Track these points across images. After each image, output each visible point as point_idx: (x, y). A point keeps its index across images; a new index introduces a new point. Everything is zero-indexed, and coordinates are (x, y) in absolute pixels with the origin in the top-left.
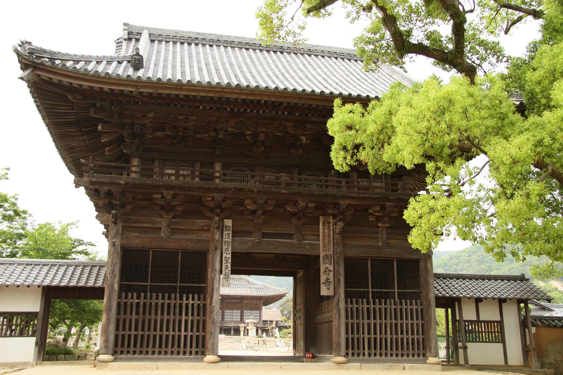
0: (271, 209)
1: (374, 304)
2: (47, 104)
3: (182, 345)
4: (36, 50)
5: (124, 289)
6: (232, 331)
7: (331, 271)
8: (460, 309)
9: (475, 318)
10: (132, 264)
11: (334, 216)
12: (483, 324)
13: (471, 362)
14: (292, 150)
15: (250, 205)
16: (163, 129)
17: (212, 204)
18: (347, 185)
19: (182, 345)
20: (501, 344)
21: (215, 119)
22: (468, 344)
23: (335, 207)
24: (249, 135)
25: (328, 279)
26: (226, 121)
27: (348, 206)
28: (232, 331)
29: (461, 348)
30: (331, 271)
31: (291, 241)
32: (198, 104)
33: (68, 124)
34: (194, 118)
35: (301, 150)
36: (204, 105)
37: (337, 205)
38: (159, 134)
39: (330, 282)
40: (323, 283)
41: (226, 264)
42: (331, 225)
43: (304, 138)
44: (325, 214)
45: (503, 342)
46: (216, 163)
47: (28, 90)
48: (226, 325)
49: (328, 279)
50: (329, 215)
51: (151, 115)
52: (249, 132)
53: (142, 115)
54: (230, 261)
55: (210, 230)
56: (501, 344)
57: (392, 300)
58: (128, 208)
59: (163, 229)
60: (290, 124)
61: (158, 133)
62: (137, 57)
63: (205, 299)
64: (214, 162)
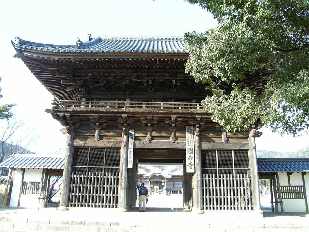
0: (156, 122)
1: (220, 177)
2: (35, 72)
3: (108, 198)
4: (23, 42)
5: (74, 169)
6: (178, 192)
7: (193, 158)
8: (278, 179)
9: (288, 185)
10: (76, 155)
11: (194, 126)
12: (285, 188)
13: (285, 211)
14: (170, 90)
15: (143, 120)
16: (98, 83)
17: (121, 121)
18: (200, 106)
19: (108, 198)
20: (304, 199)
21: (124, 74)
22: (283, 200)
23: (194, 120)
24: (145, 82)
25: (191, 163)
26: (131, 75)
27: (201, 119)
28: (178, 192)
29: (279, 202)
30: (193, 158)
31: (169, 141)
32: (111, 65)
33: (51, 83)
34: (113, 74)
35: (175, 89)
36: (115, 65)
37: (195, 119)
38: (96, 85)
39: (192, 165)
40: (188, 165)
41: (130, 155)
42: (193, 130)
43: (174, 81)
44: (189, 125)
45: (305, 198)
46: (127, 99)
47: (25, 65)
48: (175, 189)
49: (191, 163)
50: (191, 125)
51: (90, 74)
52: (144, 81)
53: (85, 74)
54: (132, 153)
55: (122, 136)
56: (304, 199)
57: (231, 175)
58: (78, 125)
59: (95, 136)
60: (167, 74)
61: (96, 84)
62: (79, 43)
63: (118, 175)
64: (126, 99)
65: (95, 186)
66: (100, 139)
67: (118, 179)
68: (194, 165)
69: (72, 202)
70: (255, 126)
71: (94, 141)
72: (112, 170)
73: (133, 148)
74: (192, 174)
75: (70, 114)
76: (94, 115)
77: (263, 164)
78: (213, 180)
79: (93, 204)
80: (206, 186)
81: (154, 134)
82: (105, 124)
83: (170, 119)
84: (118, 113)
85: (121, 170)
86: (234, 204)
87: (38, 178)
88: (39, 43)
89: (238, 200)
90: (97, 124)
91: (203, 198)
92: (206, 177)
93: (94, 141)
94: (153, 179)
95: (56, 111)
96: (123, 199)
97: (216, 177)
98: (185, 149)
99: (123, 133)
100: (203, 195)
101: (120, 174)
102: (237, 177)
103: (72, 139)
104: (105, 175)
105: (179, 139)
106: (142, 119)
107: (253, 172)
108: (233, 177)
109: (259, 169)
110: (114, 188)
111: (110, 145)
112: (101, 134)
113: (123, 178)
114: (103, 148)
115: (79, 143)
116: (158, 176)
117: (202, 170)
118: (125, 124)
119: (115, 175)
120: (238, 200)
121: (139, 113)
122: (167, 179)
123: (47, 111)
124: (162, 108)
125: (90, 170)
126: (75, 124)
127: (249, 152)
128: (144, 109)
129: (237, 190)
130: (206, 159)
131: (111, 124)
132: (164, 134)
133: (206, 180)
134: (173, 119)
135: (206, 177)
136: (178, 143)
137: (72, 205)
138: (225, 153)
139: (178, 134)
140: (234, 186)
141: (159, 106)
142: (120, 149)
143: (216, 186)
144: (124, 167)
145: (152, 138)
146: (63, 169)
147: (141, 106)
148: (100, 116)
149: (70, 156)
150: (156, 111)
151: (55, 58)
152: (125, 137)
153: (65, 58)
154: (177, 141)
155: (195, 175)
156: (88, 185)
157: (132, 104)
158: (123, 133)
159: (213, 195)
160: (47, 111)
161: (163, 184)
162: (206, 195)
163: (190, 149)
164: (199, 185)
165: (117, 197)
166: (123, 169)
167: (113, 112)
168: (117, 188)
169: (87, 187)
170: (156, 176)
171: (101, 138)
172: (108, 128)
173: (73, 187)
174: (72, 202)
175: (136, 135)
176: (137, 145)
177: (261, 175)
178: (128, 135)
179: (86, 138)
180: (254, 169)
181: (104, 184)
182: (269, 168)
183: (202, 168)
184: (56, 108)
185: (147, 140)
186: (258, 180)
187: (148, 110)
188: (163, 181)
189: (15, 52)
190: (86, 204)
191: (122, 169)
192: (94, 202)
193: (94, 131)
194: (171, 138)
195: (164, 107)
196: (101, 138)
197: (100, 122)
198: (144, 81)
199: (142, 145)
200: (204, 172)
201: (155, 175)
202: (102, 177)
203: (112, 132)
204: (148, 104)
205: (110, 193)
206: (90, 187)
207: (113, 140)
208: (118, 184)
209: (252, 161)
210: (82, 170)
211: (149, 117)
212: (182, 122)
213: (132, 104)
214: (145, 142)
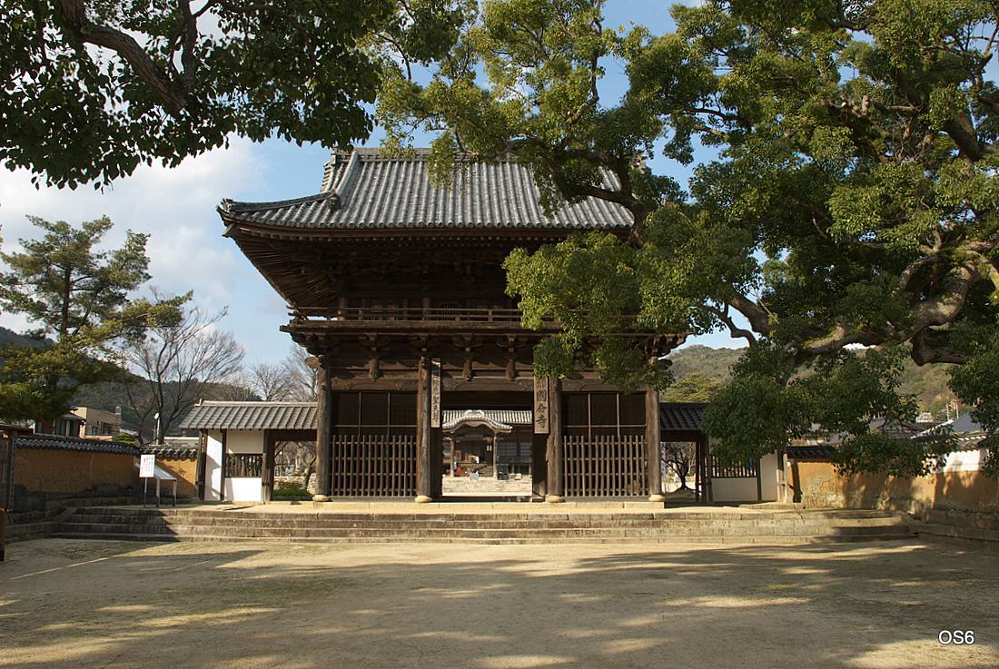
1: (593, 440)
5: (333, 431)
31: (503, 377)
51: (354, 254)
63: (415, 440)
65: (375, 459)
66: (379, 377)
67: (414, 447)
68: (547, 421)
69: (336, 487)
70: (656, 351)
71: (367, 377)
72: (403, 432)
73: (439, 391)
74: (545, 436)
75: (324, 334)
76: (368, 334)
77: (681, 415)
78: (580, 446)
79: (355, 490)
80: (568, 456)
81: (476, 366)
82: (387, 349)
83: (505, 338)
84: (412, 330)
85: (419, 430)
86: (623, 487)
87: (257, 447)
88: (262, 204)
89: (629, 482)
90: (374, 349)
91: (564, 477)
92: (568, 441)
93: (367, 377)
94: (462, 435)
95: (299, 329)
96: (426, 482)
97: (586, 440)
98: (533, 392)
99: (421, 364)
100: (564, 472)
101: (418, 437)
102: (622, 440)
103: (328, 378)
104: (391, 440)
105: (520, 373)
106: (454, 339)
107: (652, 431)
108: (616, 440)
109: (661, 423)
110: (408, 462)
111: (398, 386)
112: (381, 368)
113: (424, 445)
114: (384, 392)
115: (340, 384)
116: (476, 427)
117: (562, 428)
118: (424, 350)
119: (397, 440)
120: (629, 482)
121: (450, 330)
122: (499, 435)
123: (283, 329)
124: (490, 320)
125: (365, 432)
126: (328, 349)
127: (647, 395)
128: (457, 323)
129: (623, 462)
130: (569, 406)
131: (399, 348)
132: (491, 366)
133: (568, 446)
134: (511, 340)
135: (568, 441)
136: (520, 381)
137: (336, 494)
138: (603, 400)
139: (519, 366)
140: (616, 455)
141: (486, 316)
142: (416, 392)
143: (616, 455)
144: (425, 426)
145: (474, 373)
146: (316, 430)
147: (452, 316)
148: (379, 336)
149: (326, 407)
150: (479, 325)
151: (298, 238)
152: (425, 372)
153: (317, 236)
154: (518, 378)
155: (550, 437)
156: (363, 459)
157: (434, 313)
158: (421, 364)
159: (581, 472)
160: (283, 329)
161: (489, 448)
162: (569, 471)
163: (541, 392)
164: (557, 456)
165: (414, 478)
166: (424, 430)
167: (403, 330)
168: (415, 463)
169: (361, 461)
170: (469, 426)
171: (380, 373)
172: (390, 358)
173: (337, 462)
174: (336, 487)
175: (445, 367)
176: (446, 385)
177: (666, 436)
178: (430, 369)
179: (349, 375)
180: (653, 426)
181: (391, 456)
182: (689, 422)
183: (562, 424)
184: (299, 323)
185: (463, 376)
186: (659, 444)
187: (466, 324)
188: (489, 439)
189: (225, 229)
190: (374, 490)
191: (422, 430)
192: (590, 455)
193: (556, 491)
194: (507, 372)
195: (494, 319)
196: (380, 373)
197: (378, 345)
198: (456, 264)
199: (455, 387)
200: (564, 432)
201: (467, 423)
202: (386, 443)
203: (398, 363)
204: (463, 313)
205: (403, 471)
206: (367, 462)
207: (402, 377)
208: (415, 455)
209: (650, 413)
210: (350, 432)
211: (468, 337)
212: (527, 342)
213: (434, 313)
214: (460, 379)
